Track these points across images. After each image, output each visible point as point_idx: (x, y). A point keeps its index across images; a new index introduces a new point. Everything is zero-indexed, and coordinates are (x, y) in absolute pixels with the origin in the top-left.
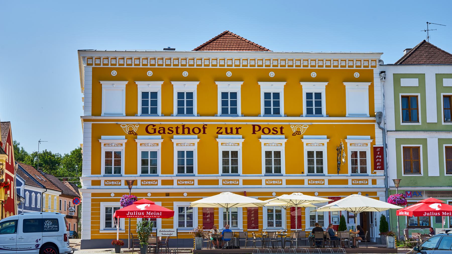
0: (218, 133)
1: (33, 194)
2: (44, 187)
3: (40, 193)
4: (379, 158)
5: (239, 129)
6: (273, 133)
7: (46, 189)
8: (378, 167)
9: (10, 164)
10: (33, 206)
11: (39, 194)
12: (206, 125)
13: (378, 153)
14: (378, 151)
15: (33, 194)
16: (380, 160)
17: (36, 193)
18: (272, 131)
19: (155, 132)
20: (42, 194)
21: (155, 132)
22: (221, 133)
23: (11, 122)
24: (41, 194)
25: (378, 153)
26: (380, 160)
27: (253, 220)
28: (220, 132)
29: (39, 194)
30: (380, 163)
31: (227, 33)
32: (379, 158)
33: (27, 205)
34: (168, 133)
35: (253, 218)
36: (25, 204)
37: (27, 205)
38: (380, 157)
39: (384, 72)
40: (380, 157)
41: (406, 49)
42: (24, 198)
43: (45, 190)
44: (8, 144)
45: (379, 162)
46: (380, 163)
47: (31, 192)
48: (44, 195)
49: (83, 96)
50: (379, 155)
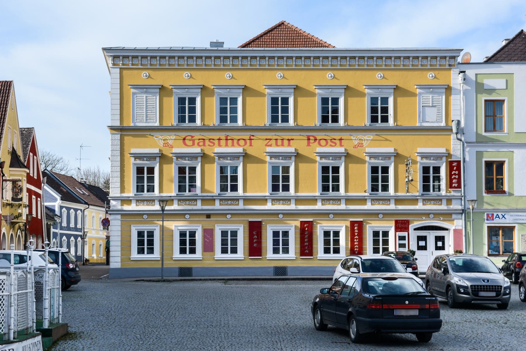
0: (266, 145)
1: (72, 211)
2: (86, 203)
3: (81, 210)
4: (455, 174)
5: (291, 141)
6: (331, 145)
7: (89, 205)
8: (454, 185)
9: (36, 177)
10: (72, 225)
11: (79, 211)
12: (253, 136)
13: (455, 168)
14: (455, 166)
15: (72, 211)
16: (457, 177)
17: (76, 210)
18: (330, 143)
19: (193, 144)
20: (83, 211)
21: (193, 144)
22: (271, 146)
23: (35, 128)
24: (82, 212)
25: (455, 168)
26: (457, 177)
27: (306, 246)
28: (269, 144)
29: (79, 211)
30: (456, 180)
31: (283, 23)
32: (455, 174)
33: (64, 224)
34: (209, 145)
35: (306, 244)
36: (61, 223)
37: (64, 224)
38: (457, 172)
39: (464, 72)
40: (457, 172)
41: (506, 40)
42: (61, 216)
43: (87, 206)
44: (31, 154)
45: (455, 178)
46: (456, 180)
47: (68, 209)
48: (86, 212)
49: (226, 47)
50: (455, 171)
